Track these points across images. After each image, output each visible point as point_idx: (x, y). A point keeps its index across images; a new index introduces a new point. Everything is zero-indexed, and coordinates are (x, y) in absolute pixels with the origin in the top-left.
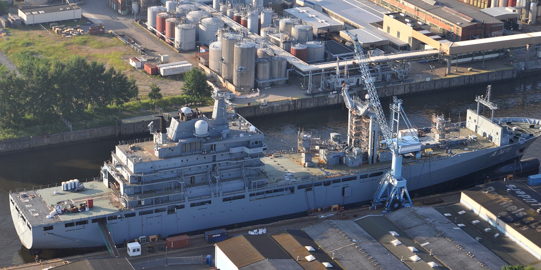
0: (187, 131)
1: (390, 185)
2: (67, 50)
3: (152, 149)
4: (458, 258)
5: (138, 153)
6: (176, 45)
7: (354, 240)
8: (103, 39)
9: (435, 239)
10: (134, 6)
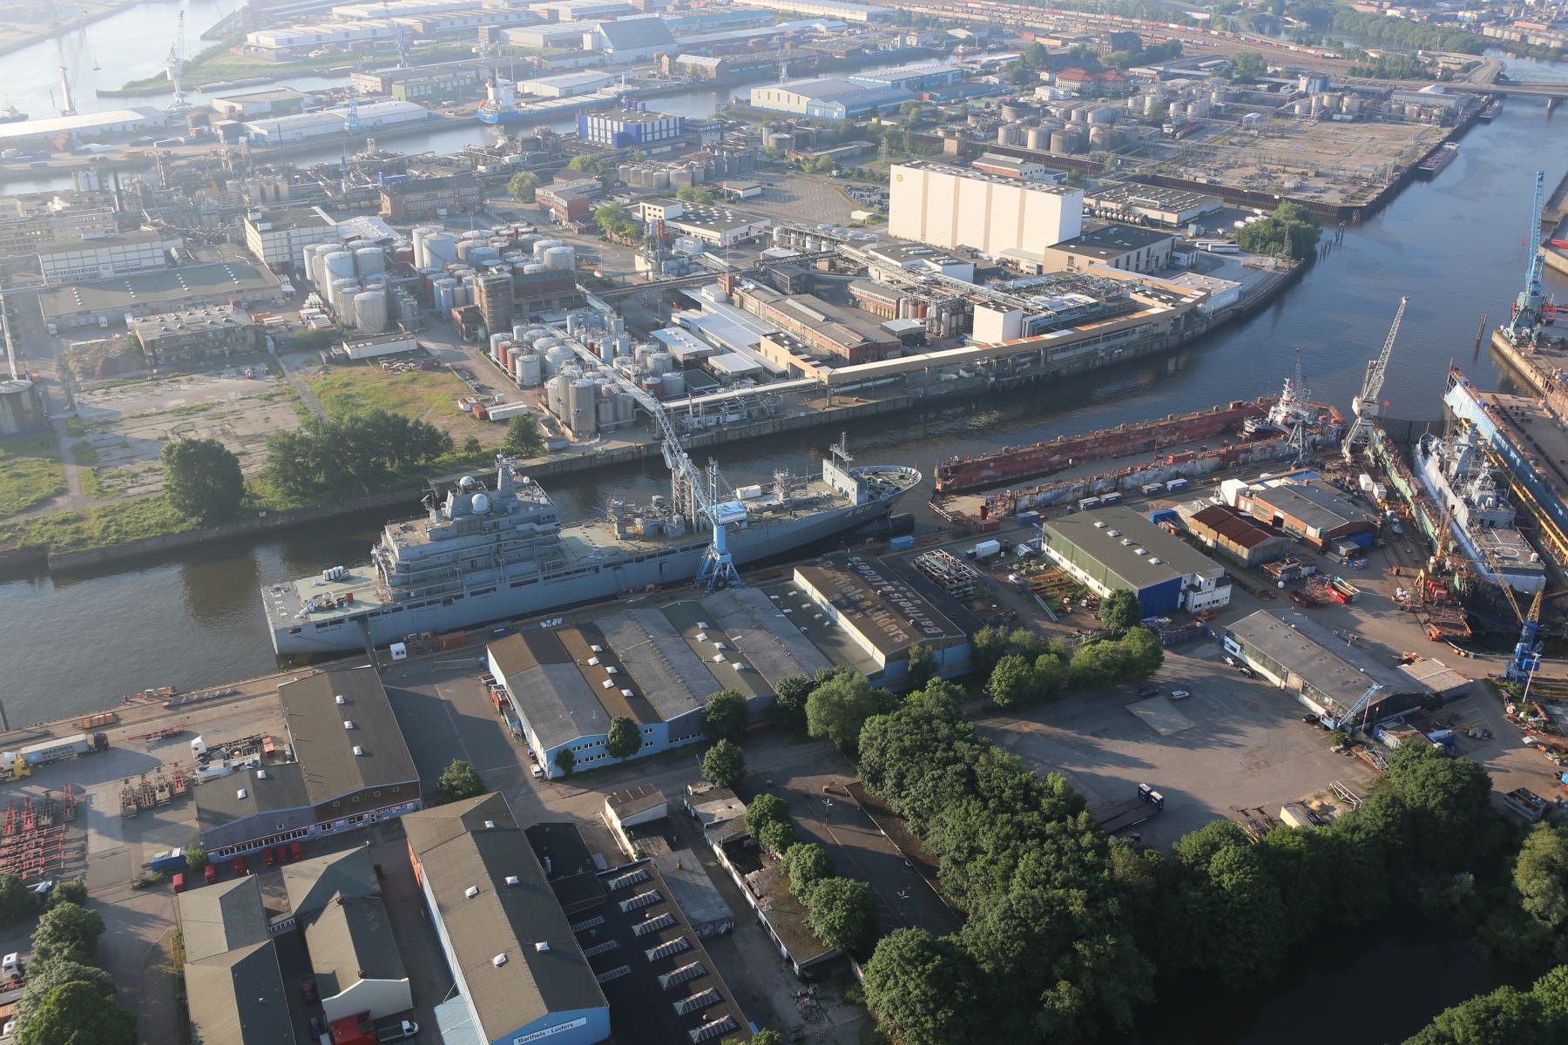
0: (463, 508)
3: (421, 532)
5: (409, 535)
8: (437, 374)
10: (481, 332)
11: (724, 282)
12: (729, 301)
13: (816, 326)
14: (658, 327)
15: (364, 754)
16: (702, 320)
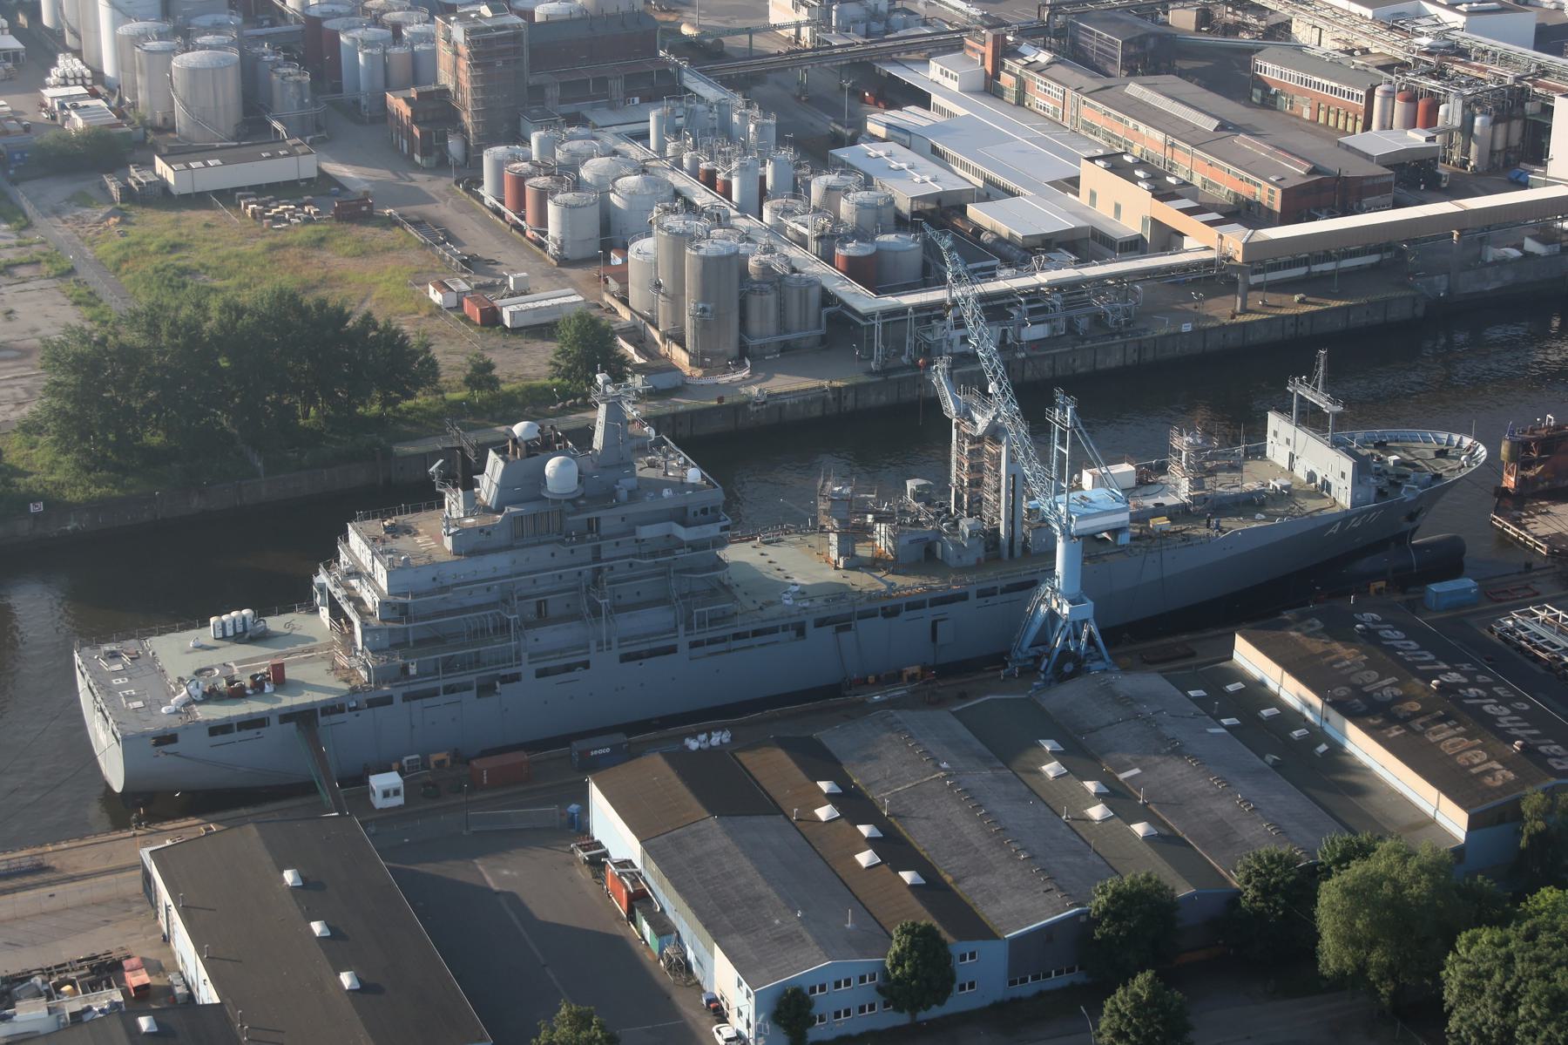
0: (524, 485)
1: (1053, 616)
2: (272, 262)
3: (435, 536)
4: (1211, 811)
5: (403, 543)
6: (552, 247)
7: (945, 765)
8: (368, 231)
9: (1157, 759)
10: (454, 145)
11: (981, 50)
12: (991, 88)
13: (1199, 141)
14: (839, 141)
15: (365, 988)
16: (936, 129)
